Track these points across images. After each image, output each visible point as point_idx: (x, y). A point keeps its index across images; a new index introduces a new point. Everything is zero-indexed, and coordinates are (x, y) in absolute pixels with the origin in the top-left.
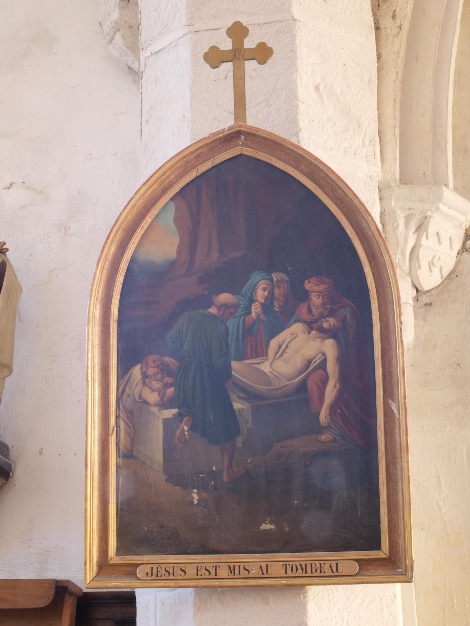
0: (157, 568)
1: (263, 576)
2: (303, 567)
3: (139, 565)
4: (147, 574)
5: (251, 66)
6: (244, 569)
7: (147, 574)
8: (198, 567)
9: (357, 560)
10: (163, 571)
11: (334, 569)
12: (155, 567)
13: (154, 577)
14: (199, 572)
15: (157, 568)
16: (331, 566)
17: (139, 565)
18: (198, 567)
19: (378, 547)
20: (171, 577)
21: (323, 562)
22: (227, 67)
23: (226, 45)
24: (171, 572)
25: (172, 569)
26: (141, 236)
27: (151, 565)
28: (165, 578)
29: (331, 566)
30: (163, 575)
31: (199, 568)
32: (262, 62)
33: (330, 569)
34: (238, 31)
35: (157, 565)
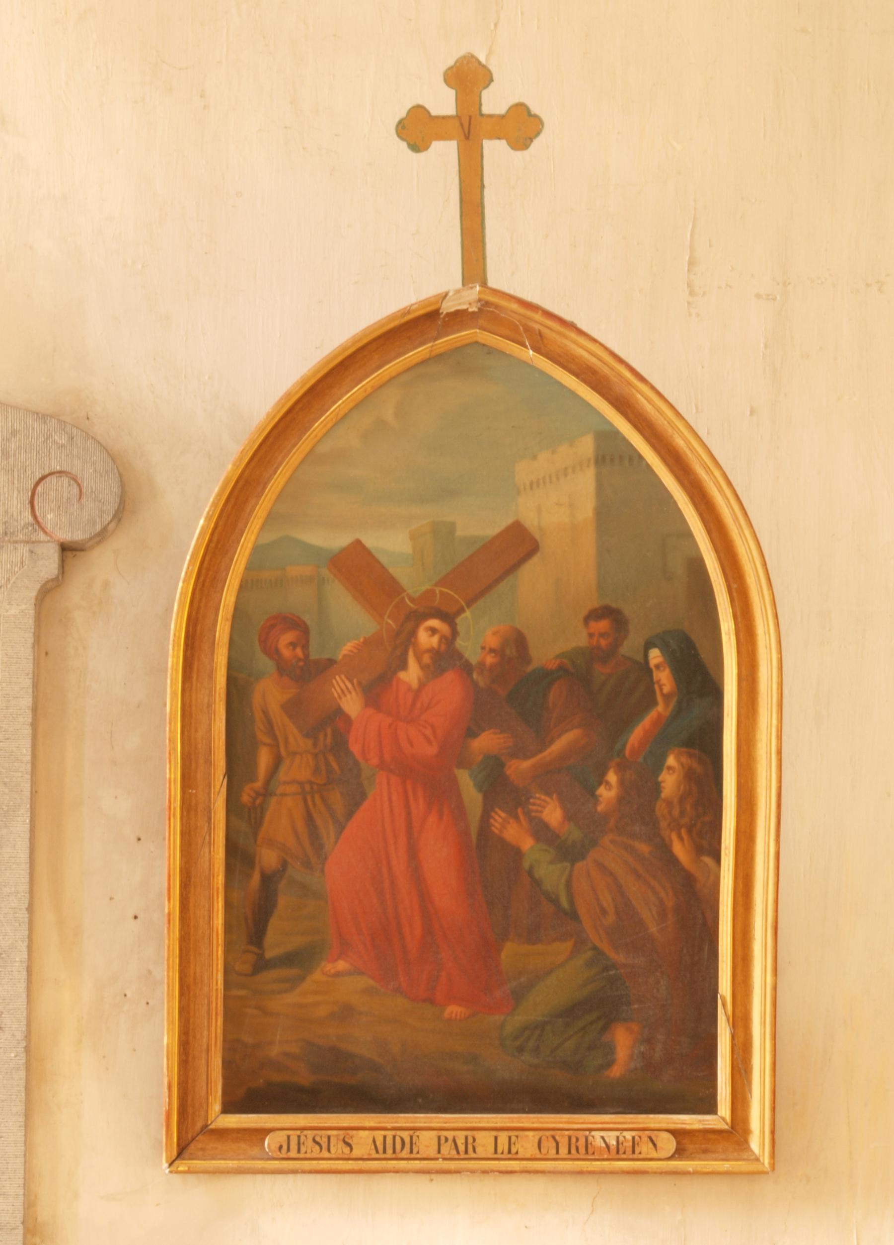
0: (299, 1137)
1: (377, 1156)
2: (378, 1143)
3: (268, 1131)
4: (281, 1147)
5: (495, 151)
6: (314, 1140)
7: (281, 1147)
8: (510, 1138)
9: (673, 1132)
10: (310, 1142)
11: (462, 1148)
12: (294, 1135)
13: (293, 1154)
14: (512, 1146)
15: (299, 1137)
16: (374, 1141)
17: (268, 1131)
18: (510, 1138)
19: (710, 1107)
20: (325, 1154)
21: (516, 1133)
22: (445, 152)
23: (494, 102)
24: (325, 1145)
25: (325, 1140)
26: (274, 497)
27: (567, 1133)
28: (314, 1155)
29: (374, 1141)
30: (309, 1151)
31: (513, 1139)
32: (418, 112)
33: (373, 1147)
34: (522, 126)
35: (298, 1132)
